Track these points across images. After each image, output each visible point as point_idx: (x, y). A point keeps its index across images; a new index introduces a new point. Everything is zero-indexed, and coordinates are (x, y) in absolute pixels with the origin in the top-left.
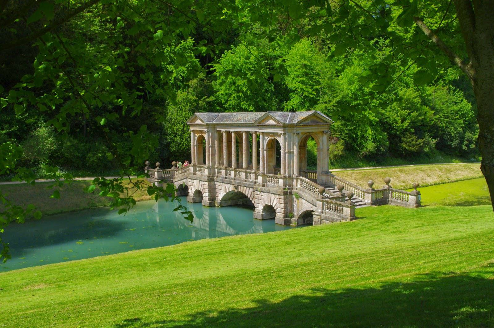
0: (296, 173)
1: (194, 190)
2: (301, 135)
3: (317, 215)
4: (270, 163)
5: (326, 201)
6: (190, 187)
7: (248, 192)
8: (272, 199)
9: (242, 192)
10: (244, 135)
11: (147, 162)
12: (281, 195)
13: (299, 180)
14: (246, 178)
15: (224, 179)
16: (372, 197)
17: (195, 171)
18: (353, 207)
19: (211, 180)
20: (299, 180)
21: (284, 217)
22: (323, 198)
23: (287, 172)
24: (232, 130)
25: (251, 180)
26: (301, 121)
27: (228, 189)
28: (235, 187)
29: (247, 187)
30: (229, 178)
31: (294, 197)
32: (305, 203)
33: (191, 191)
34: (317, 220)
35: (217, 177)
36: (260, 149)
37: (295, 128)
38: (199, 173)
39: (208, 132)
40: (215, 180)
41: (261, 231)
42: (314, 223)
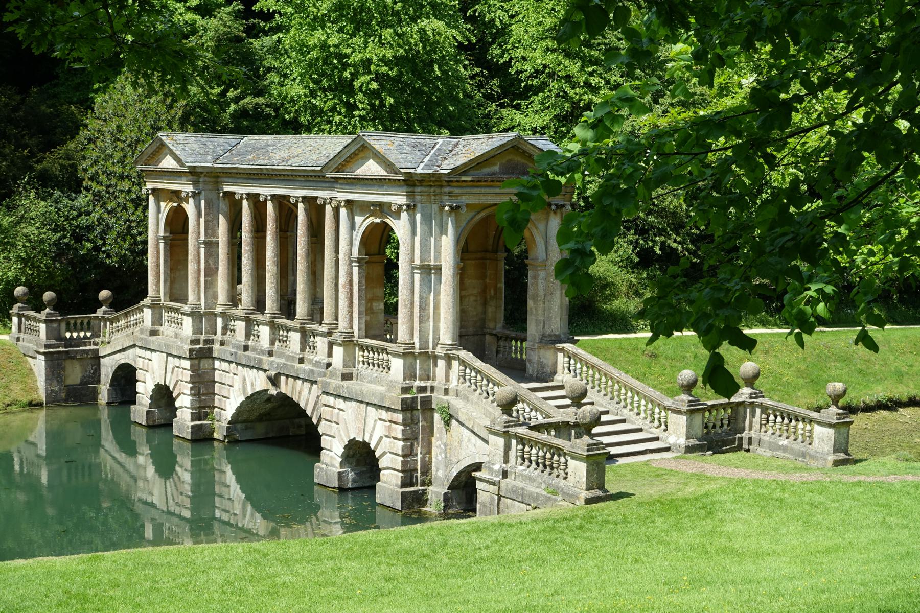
0: (446, 336)
1: (150, 386)
2: (466, 215)
3: (488, 482)
4: (374, 304)
5: (516, 436)
6: (139, 375)
7: (305, 396)
8: (370, 423)
9: (289, 395)
10: (270, 207)
11: (19, 290)
12: (395, 411)
13: (455, 363)
14: (303, 350)
15: (241, 352)
16: (689, 427)
17: (157, 321)
18: (599, 461)
19: (201, 356)
20: (455, 363)
21: (403, 485)
22: (508, 424)
23: (416, 334)
24: (265, 191)
25: (317, 358)
26: (464, 165)
27: (252, 385)
28: (270, 378)
29: (305, 380)
30: (254, 350)
31: (437, 416)
32: (469, 441)
33: (145, 389)
34: (489, 499)
35: (222, 343)
36: (341, 256)
37: (447, 189)
38: (167, 329)
39: (195, 195)
40: (215, 355)
41: (337, 531)
42: (478, 506)
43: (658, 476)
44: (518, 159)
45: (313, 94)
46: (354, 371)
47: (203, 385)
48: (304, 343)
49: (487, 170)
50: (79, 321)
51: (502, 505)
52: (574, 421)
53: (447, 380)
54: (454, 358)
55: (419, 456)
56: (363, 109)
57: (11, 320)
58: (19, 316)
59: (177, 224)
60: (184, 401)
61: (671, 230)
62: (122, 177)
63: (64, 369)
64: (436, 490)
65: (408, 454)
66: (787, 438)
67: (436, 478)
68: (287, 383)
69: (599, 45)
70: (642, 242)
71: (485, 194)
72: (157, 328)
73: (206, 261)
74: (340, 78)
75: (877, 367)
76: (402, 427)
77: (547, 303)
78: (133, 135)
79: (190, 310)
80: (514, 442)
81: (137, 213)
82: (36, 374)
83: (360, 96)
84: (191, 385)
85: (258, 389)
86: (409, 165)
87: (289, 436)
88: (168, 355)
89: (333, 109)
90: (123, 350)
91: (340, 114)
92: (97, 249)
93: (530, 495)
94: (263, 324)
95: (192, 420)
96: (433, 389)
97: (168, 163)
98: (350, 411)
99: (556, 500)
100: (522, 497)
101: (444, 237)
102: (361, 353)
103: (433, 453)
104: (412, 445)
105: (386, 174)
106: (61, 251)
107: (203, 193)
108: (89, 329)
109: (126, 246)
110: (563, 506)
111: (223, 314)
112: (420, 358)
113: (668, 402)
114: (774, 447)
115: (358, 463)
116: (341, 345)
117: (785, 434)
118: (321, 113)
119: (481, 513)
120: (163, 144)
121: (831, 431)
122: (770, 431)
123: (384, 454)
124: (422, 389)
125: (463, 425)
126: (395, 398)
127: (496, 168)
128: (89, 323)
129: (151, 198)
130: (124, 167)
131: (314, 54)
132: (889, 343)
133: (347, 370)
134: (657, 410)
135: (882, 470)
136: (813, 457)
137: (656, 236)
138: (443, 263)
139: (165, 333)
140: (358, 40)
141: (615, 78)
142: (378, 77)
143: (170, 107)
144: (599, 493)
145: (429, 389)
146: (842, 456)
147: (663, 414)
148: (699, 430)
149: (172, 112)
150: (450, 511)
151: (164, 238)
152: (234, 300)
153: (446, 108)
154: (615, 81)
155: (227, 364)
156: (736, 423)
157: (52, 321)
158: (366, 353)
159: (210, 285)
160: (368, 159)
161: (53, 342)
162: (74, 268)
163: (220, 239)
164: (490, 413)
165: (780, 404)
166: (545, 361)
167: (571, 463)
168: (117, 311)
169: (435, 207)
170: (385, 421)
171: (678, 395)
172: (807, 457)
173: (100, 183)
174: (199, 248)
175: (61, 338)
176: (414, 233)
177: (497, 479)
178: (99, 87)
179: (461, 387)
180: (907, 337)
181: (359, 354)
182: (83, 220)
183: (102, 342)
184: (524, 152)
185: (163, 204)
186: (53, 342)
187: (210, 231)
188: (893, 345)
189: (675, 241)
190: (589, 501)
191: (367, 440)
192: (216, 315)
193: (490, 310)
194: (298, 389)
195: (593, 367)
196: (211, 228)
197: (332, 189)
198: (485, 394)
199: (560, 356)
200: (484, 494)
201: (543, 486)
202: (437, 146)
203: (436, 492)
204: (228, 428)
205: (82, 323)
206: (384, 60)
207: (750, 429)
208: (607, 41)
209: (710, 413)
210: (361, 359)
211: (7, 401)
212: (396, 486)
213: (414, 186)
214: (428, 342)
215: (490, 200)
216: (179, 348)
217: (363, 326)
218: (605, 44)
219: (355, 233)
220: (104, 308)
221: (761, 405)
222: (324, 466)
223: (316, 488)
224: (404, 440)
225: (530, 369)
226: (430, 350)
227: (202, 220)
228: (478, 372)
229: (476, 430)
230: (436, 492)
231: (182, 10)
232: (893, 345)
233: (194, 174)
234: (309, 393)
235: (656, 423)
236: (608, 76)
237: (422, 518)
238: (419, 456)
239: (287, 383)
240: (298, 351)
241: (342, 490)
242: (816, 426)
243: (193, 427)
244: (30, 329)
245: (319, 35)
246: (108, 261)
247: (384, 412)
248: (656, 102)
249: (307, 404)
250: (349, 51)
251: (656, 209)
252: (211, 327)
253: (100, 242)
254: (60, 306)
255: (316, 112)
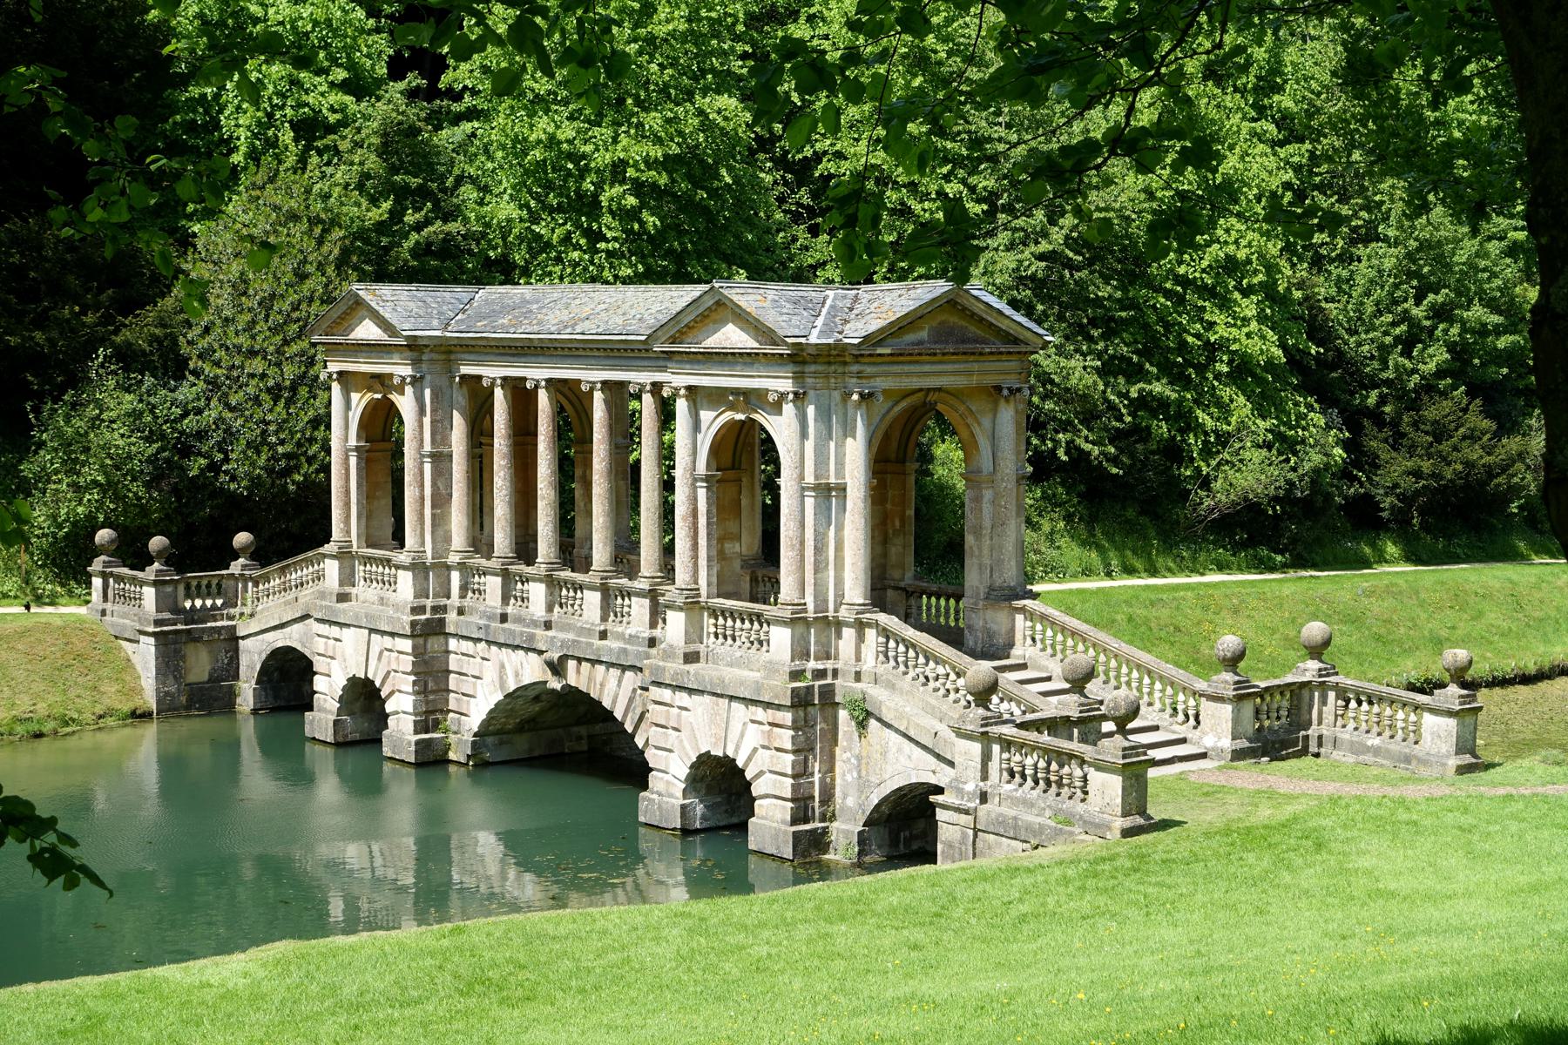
0: (855, 588)
1: (339, 681)
2: (881, 404)
4: (727, 546)
6: (319, 664)
7: (612, 691)
10: (598, 396)
11: (103, 535)
12: (779, 707)
13: (871, 634)
14: (604, 619)
15: (496, 625)
16: (1236, 721)
17: (348, 578)
18: (1134, 772)
19: (429, 630)
21: (794, 822)
22: (986, 722)
23: (809, 590)
24: (536, 373)
26: (881, 330)
27: (517, 675)
29: (611, 665)
30: (519, 620)
31: (843, 715)
32: (900, 750)
33: (328, 687)
34: (958, 836)
35: (461, 612)
37: (855, 368)
38: (365, 593)
39: (416, 381)
40: (450, 629)
41: (679, 894)
42: (940, 847)
43: (1207, 794)
44: (954, 319)
45: (535, 219)
46: (702, 648)
47: (432, 678)
48: (607, 608)
49: (910, 337)
50: (204, 582)
51: (979, 844)
52: (1078, 715)
53: (858, 659)
54: (869, 625)
55: (817, 778)
56: (615, 239)
57: (89, 584)
58: (104, 576)
59: (381, 428)
60: (401, 705)
61: (1081, 422)
62: (252, 353)
63: (183, 658)
64: (843, 827)
65: (801, 772)
66: (1379, 734)
67: (842, 809)
68: (578, 671)
69: (959, 133)
70: (1035, 441)
71: (908, 374)
72: (347, 589)
73: (434, 484)
74: (577, 191)
75: (1402, 630)
76: (792, 732)
77: (995, 538)
78: (265, 286)
79: (409, 560)
80: (996, 748)
81: (278, 409)
82: (139, 668)
83: (607, 219)
84: (413, 678)
85: (527, 680)
86: (797, 332)
87: (563, 754)
88: (372, 631)
89: (566, 239)
90: (282, 626)
91: (577, 247)
92: (214, 467)
93: (1029, 828)
94: (535, 580)
95: (416, 732)
96: (835, 673)
97: (367, 331)
98: (700, 710)
99: (1072, 833)
100: (1013, 830)
101: (849, 440)
102: (712, 621)
103: (838, 770)
104: (806, 760)
105: (756, 345)
106: (158, 473)
107: (428, 377)
108: (219, 594)
109: (262, 462)
110: (1089, 844)
111: (462, 567)
112: (816, 627)
113: (1201, 685)
114: (1358, 749)
115: (710, 790)
116: (681, 609)
117: (1375, 729)
118: (548, 245)
119: (945, 858)
120: (359, 303)
121: (1452, 723)
122: (1352, 725)
123: (761, 773)
124: (820, 674)
125: (888, 726)
126: (781, 688)
127: (923, 334)
128: (219, 585)
129: (336, 387)
130: (253, 337)
131: (537, 154)
132: (1417, 593)
133: (692, 648)
134: (1181, 697)
135: (1525, 776)
136: (1423, 762)
137: (1057, 432)
138: (848, 480)
139: (361, 598)
140: (603, 132)
141: (984, 183)
142: (638, 188)
143: (320, 242)
144: (1140, 821)
145: (830, 674)
146: (1468, 759)
147: (1192, 702)
148: (1250, 726)
149: (325, 249)
150: (868, 859)
151: (357, 449)
152: (480, 541)
153: (738, 237)
154: (985, 188)
155: (470, 644)
156: (1298, 715)
157: (165, 582)
158: (721, 621)
159: (440, 521)
160: (724, 323)
161: (167, 615)
162: (179, 499)
163: (454, 449)
164: (933, 708)
165: (1366, 685)
166: (994, 627)
167: (1093, 775)
168: (263, 566)
169: (837, 395)
170: (761, 723)
171: (1217, 672)
172: (1414, 762)
173: (217, 364)
174: (422, 463)
175: (177, 610)
176: (804, 435)
177: (972, 805)
178: (196, 210)
179: (881, 669)
180: (1443, 583)
181: (708, 622)
182: (189, 423)
183: (242, 614)
184: (964, 309)
185: (355, 396)
186: (167, 615)
187: (438, 437)
188: (1423, 596)
189: (1087, 441)
190: (1128, 833)
191: (730, 754)
192: (449, 568)
193: (894, 551)
194: (599, 679)
195: (1073, 634)
196: (441, 431)
197: (663, 369)
198: (922, 679)
199: (1019, 618)
200: (949, 828)
201: (1048, 813)
202: (829, 302)
203: (845, 831)
204: (474, 743)
205: (209, 586)
206: (650, 163)
207: (1320, 723)
208: (973, 128)
209: (1263, 699)
210: (712, 629)
211: (99, 710)
212: (783, 822)
213: (804, 363)
214: (826, 601)
215: (915, 383)
216: (391, 620)
217: (715, 580)
218: (969, 132)
219: (700, 437)
220: (241, 560)
221: (1336, 687)
222: (655, 796)
223: (642, 830)
224: (795, 752)
225: (970, 641)
226: (831, 614)
227: (427, 420)
228: (909, 645)
229: (912, 734)
230: (845, 831)
231: (324, 88)
232: (1423, 596)
233: (415, 348)
234: (619, 684)
235: (1181, 717)
236: (972, 180)
237: (825, 872)
238: (817, 778)
239: (578, 671)
240: (598, 621)
241: (686, 832)
242: (1426, 716)
243: (418, 743)
244: (124, 597)
245: (543, 124)
246: (233, 486)
247: (760, 710)
248: (1053, 222)
249: (614, 702)
250: (588, 148)
251: (1055, 390)
252: (441, 586)
253: (220, 456)
254: (179, 560)
255: (539, 245)
